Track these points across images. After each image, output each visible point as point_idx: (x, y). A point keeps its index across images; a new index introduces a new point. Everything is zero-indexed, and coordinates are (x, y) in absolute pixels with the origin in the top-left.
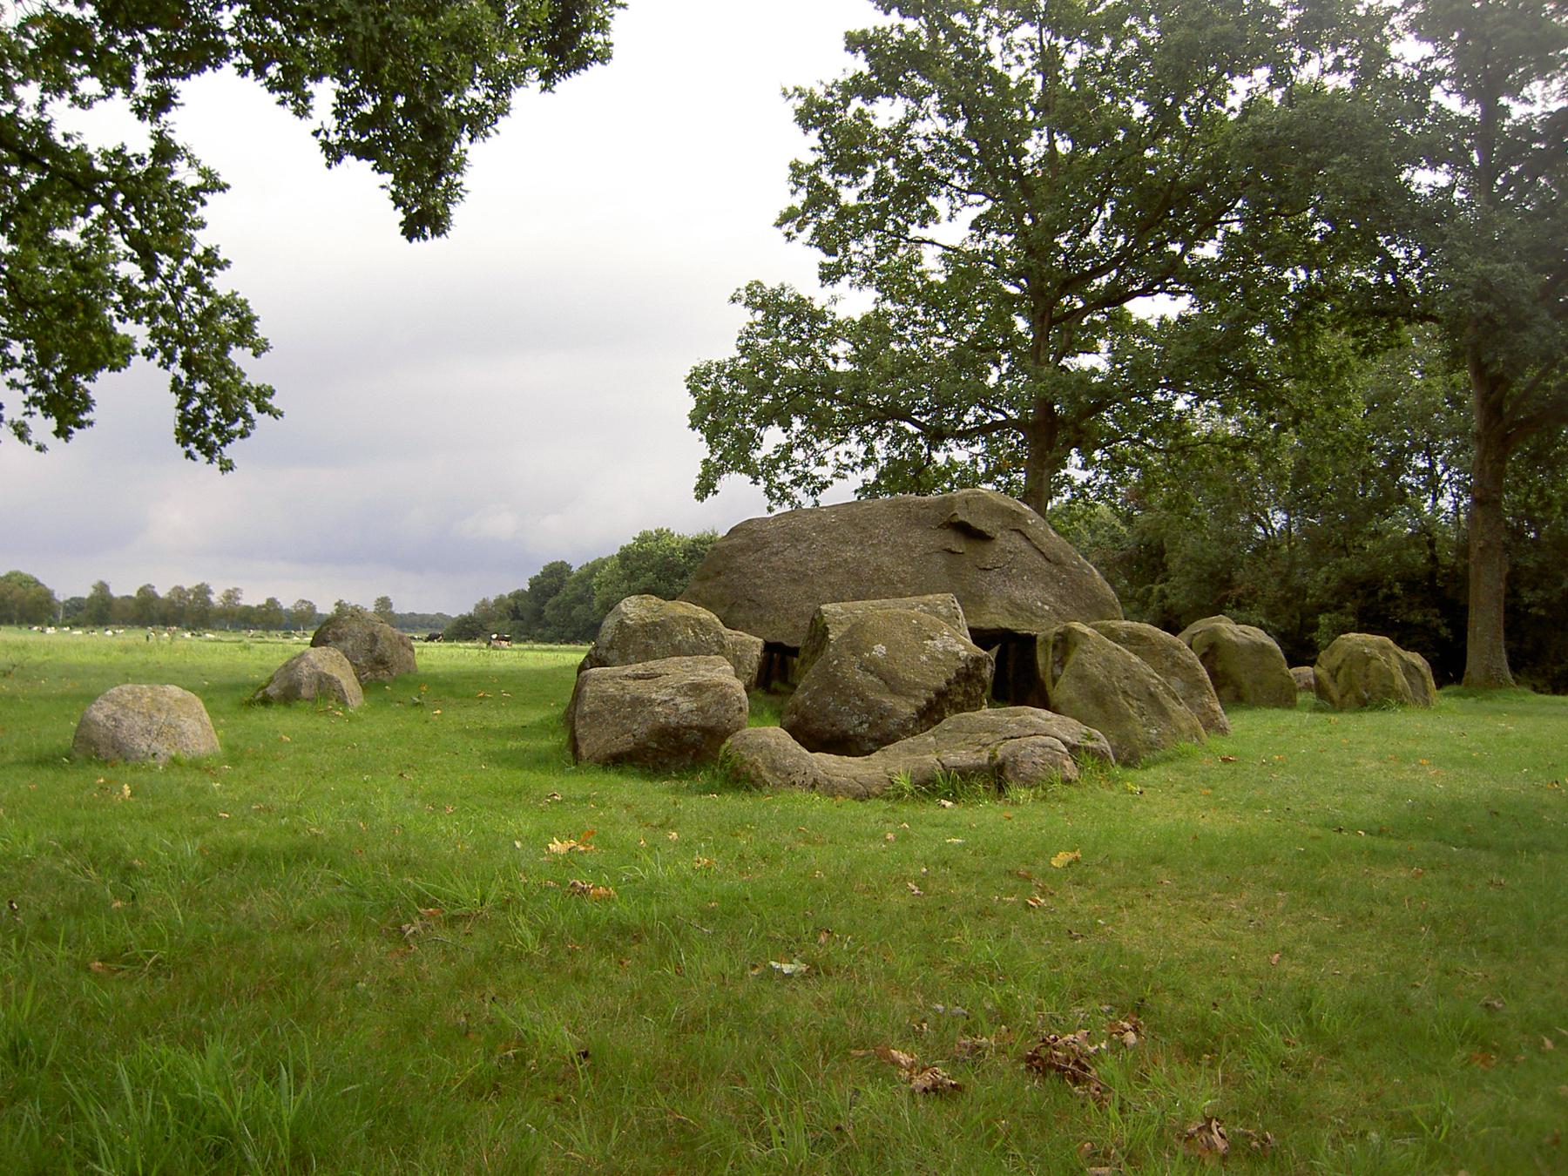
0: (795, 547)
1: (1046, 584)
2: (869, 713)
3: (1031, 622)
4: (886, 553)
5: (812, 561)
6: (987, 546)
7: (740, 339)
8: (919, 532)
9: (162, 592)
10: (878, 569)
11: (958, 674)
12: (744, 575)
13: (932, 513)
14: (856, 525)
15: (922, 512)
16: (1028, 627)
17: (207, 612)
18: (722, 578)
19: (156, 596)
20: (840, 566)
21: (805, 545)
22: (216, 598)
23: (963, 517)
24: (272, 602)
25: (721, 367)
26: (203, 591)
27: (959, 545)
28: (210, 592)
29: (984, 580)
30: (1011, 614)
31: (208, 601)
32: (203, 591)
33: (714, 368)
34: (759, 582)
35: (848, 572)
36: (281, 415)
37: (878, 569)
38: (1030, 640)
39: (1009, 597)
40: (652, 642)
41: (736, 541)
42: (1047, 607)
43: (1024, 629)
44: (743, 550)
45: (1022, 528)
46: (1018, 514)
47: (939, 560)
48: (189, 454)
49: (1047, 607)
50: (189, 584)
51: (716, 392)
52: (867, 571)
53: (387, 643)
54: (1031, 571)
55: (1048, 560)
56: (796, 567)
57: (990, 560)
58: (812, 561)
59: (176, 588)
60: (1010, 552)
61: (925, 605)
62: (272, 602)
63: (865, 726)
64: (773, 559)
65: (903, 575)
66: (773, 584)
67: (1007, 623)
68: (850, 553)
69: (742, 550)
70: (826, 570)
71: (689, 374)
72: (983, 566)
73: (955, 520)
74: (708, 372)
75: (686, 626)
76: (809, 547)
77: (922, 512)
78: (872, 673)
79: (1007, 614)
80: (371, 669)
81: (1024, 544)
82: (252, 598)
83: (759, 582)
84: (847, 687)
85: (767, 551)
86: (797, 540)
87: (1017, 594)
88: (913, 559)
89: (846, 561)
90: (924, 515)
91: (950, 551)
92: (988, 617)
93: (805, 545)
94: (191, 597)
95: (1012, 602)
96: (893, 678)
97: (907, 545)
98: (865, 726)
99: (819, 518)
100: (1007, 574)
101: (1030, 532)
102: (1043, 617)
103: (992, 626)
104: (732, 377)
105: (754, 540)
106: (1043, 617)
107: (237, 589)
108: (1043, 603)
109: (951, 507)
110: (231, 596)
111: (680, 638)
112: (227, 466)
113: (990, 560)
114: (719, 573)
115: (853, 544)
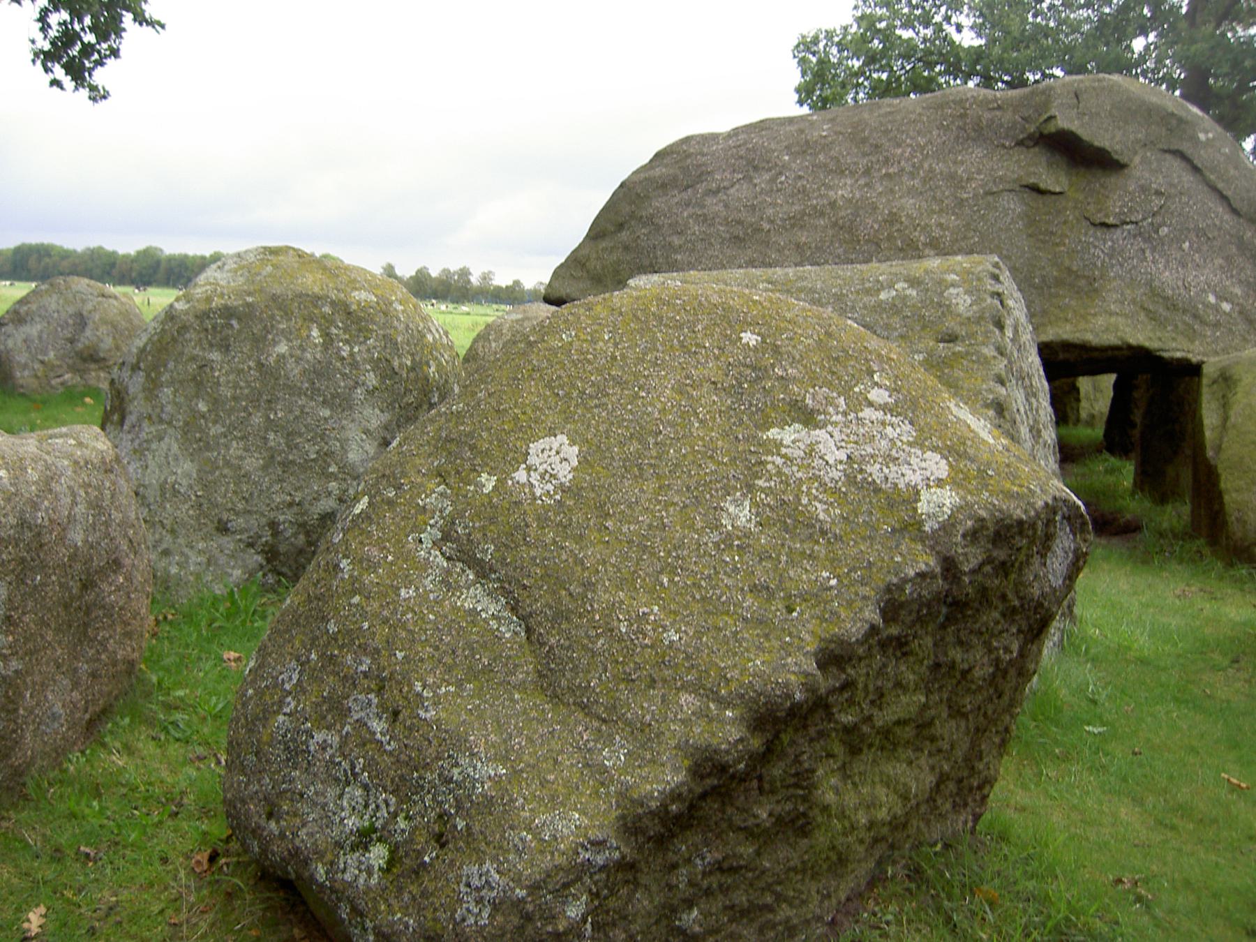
0: (751, 179)
1: (1228, 259)
2: (405, 790)
3: (1192, 335)
4: (911, 192)
5: (774, 205)
6: (1113, 180)
7: (856, 7)
8: (979, 152)
9: (434, 273)
10: (893, 219)
11: (891, 610)
12: (658, 228)
13: (1007, 117)
14: (864, 141)
15: (987, 115)
16: (1185, 344)
17: (467, 290)
18: (624, 235)
19: (429, 275)
20: (822, 214)
21: (767, 176)
22: (475, 280)
23: (1066, 121)
24: (517, 283)
25: (829, 35)
26: (464, 273)
27: (1051, 176)
28: (470, 274)
29: (1101, 246)
30: (1152, 316)
31: (469, 281)
32: (464, 273)
33: (822, 36)
34: (676, 241)
35: (835, 224)
36: (163, 26)
37: (893, 219)
38: (1192, 370)
39: (1149, 283)
40: (215, 356)
41: (657, 172)
42: (1226, 307)
43: (1175, 347)
44: (664, 186)
45: (1185, 147)
46: (1181, 120)
47: (1013, 205)
48: (56, 83)
49: (1226, 307)
50: (454, 267)
51: (823, 62)
52: (870, 224)
53: (103, 329)
54: (1201, 233)
55: (1235, 211)
56: (743, 215)
57: (1114, 206)
58: (774, 205)
59: (444, 270)
60: (1158, 193)
61: (913, 282)
62: (517, 283)
63: (378, 854)
64: (709, 201)
65: (937, 233)
66: (699, 246)
67: (1140, 335)
68: (843, 190)
69: (664, 186)
70: (796, 222)
71: (796, 43)
72: (1099, 218)
73: (1051, 128)
74: (816, 41)
75: (310, 319)
76: (773, 180)
77: (987, 115)
78: (483, 571)
79: (1142, 317)
80: (73, 369)
81: (1188, 179)
82: (502, 280)
83: (676, 241)
84: (349, 638)
85: (701, 188)
86: (756, 168)
87: (1167, 277)
88: (961, 203)
89: (833, 204)
90: (992, 121)
91: (1036, 190)
92: (1101, 321)
93: (767, 176)
94: (456, 277)
95: (1155, 293)
96: (561, 615)
97: (952, 176)
98: (378, 854)
99: (802, 131)
100: (1149, 236)
101: (1201, 157)
102: (1217, 325)
103: (1110, 339)
104: (841, 47)
105: (685, 170)
106: (1217, 325)
107: (490, 272)
108: (1221, 298)
109: (1046, 105)
110: (486, 277)
111: (282, 348)
112: (98, 95)
113: (1114, 206)
114: (621, 226)
115: (852, 173)
